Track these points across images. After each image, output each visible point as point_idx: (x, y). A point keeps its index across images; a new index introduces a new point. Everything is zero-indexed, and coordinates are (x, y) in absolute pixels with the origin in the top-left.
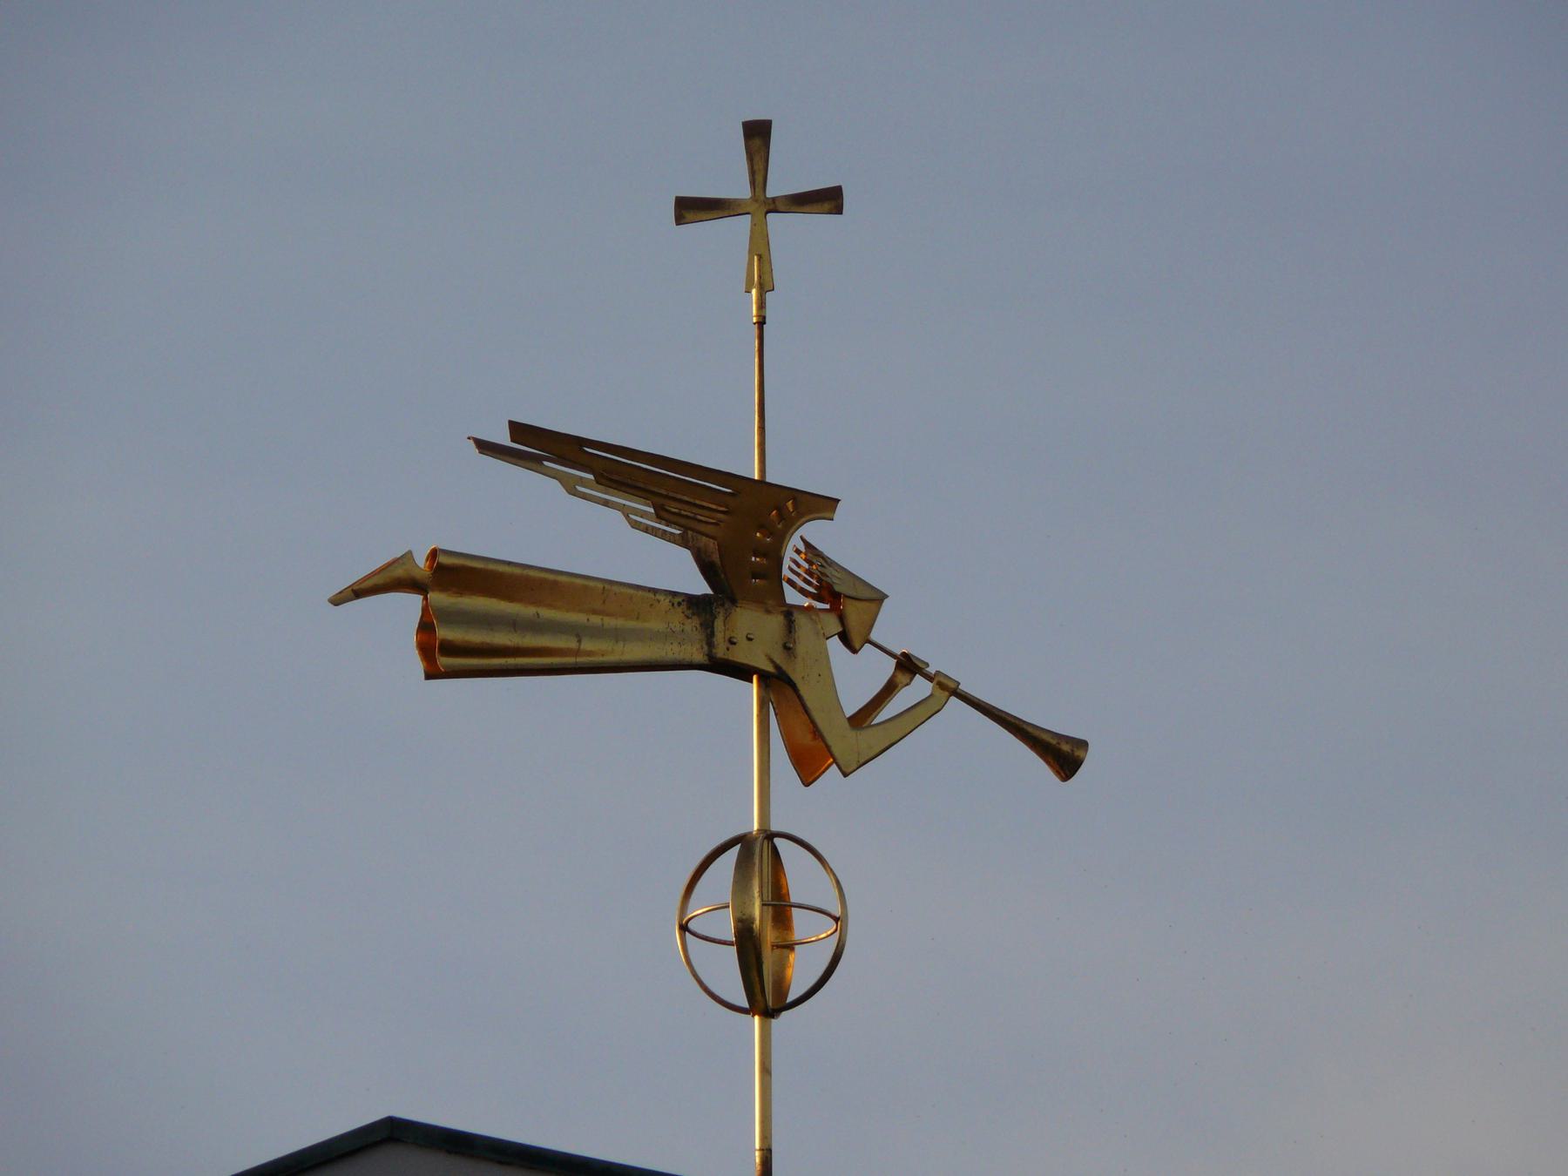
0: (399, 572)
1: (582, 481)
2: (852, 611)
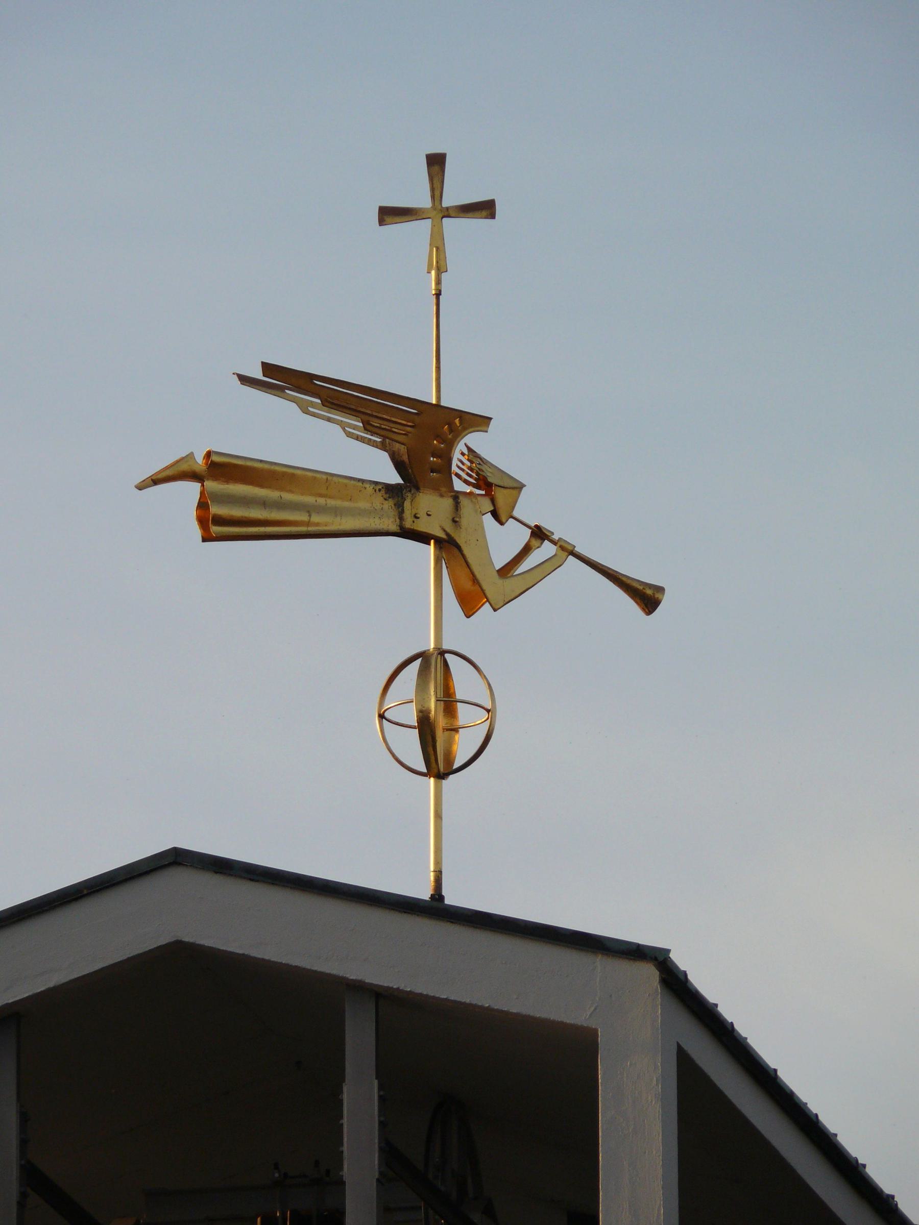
0: (184, 467)
1: (313, 405)
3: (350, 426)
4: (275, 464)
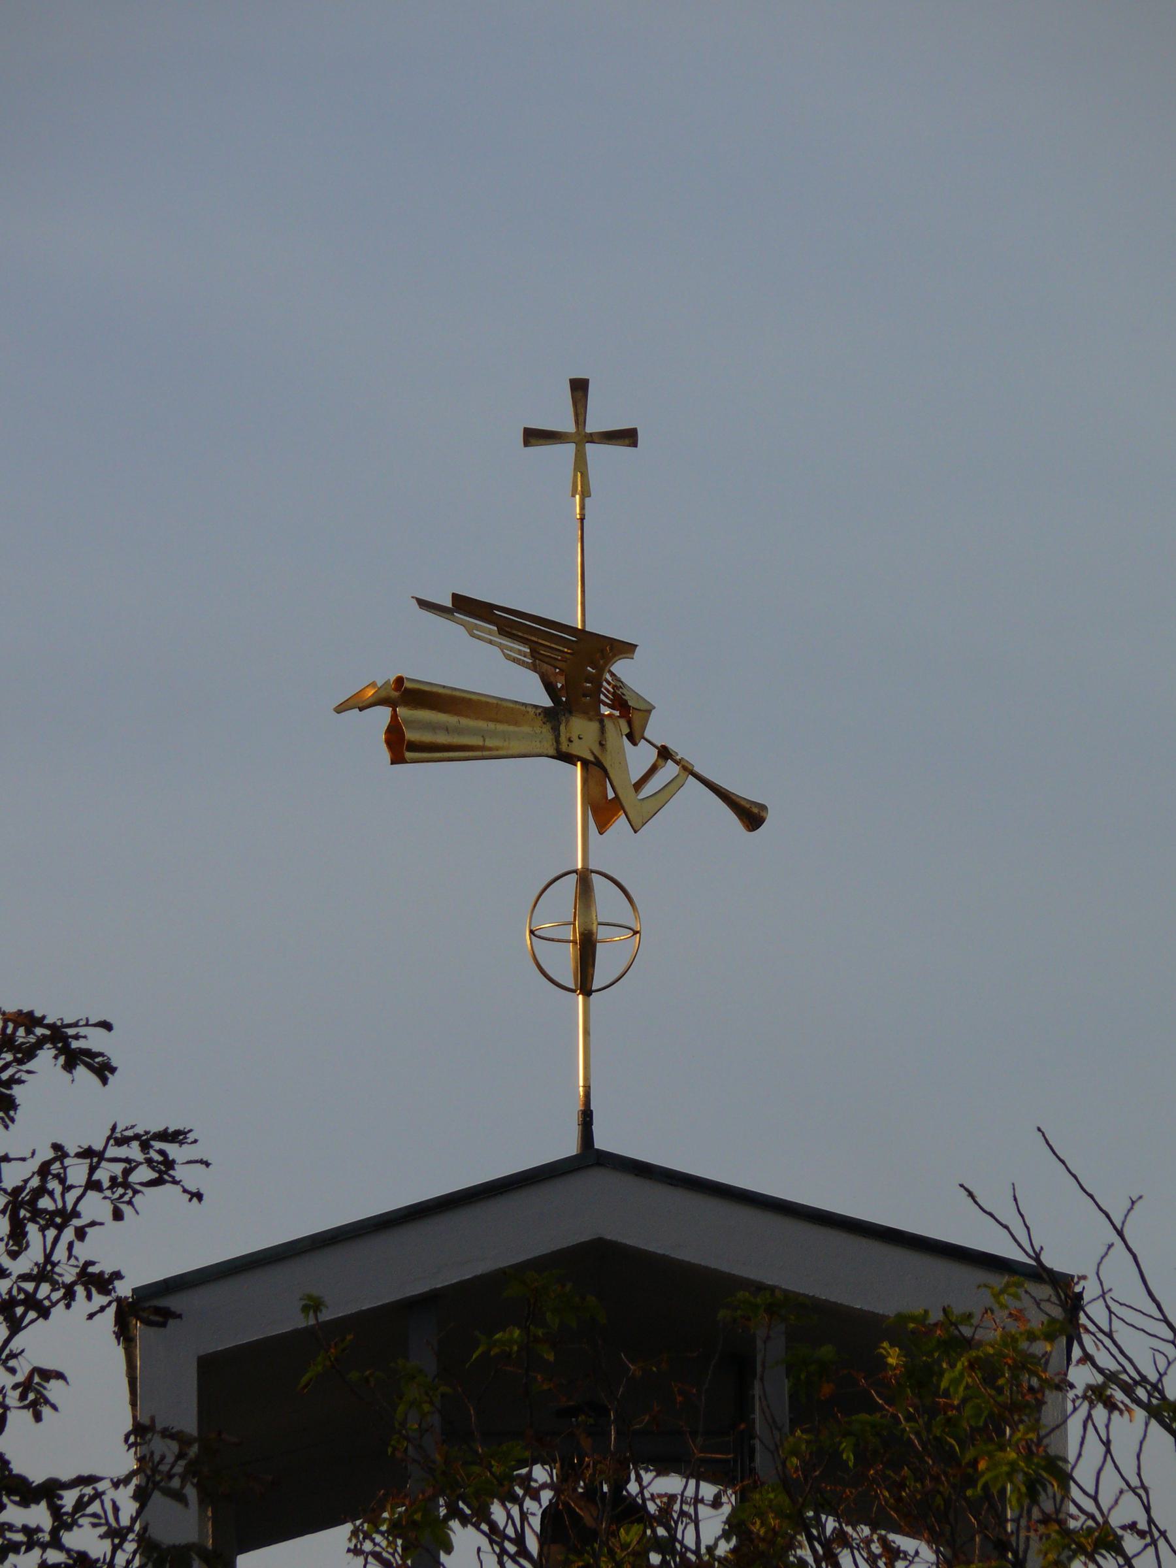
1: (477, 627)
2: (636, 718)
3: (511, 649)
4: (455, 689)
